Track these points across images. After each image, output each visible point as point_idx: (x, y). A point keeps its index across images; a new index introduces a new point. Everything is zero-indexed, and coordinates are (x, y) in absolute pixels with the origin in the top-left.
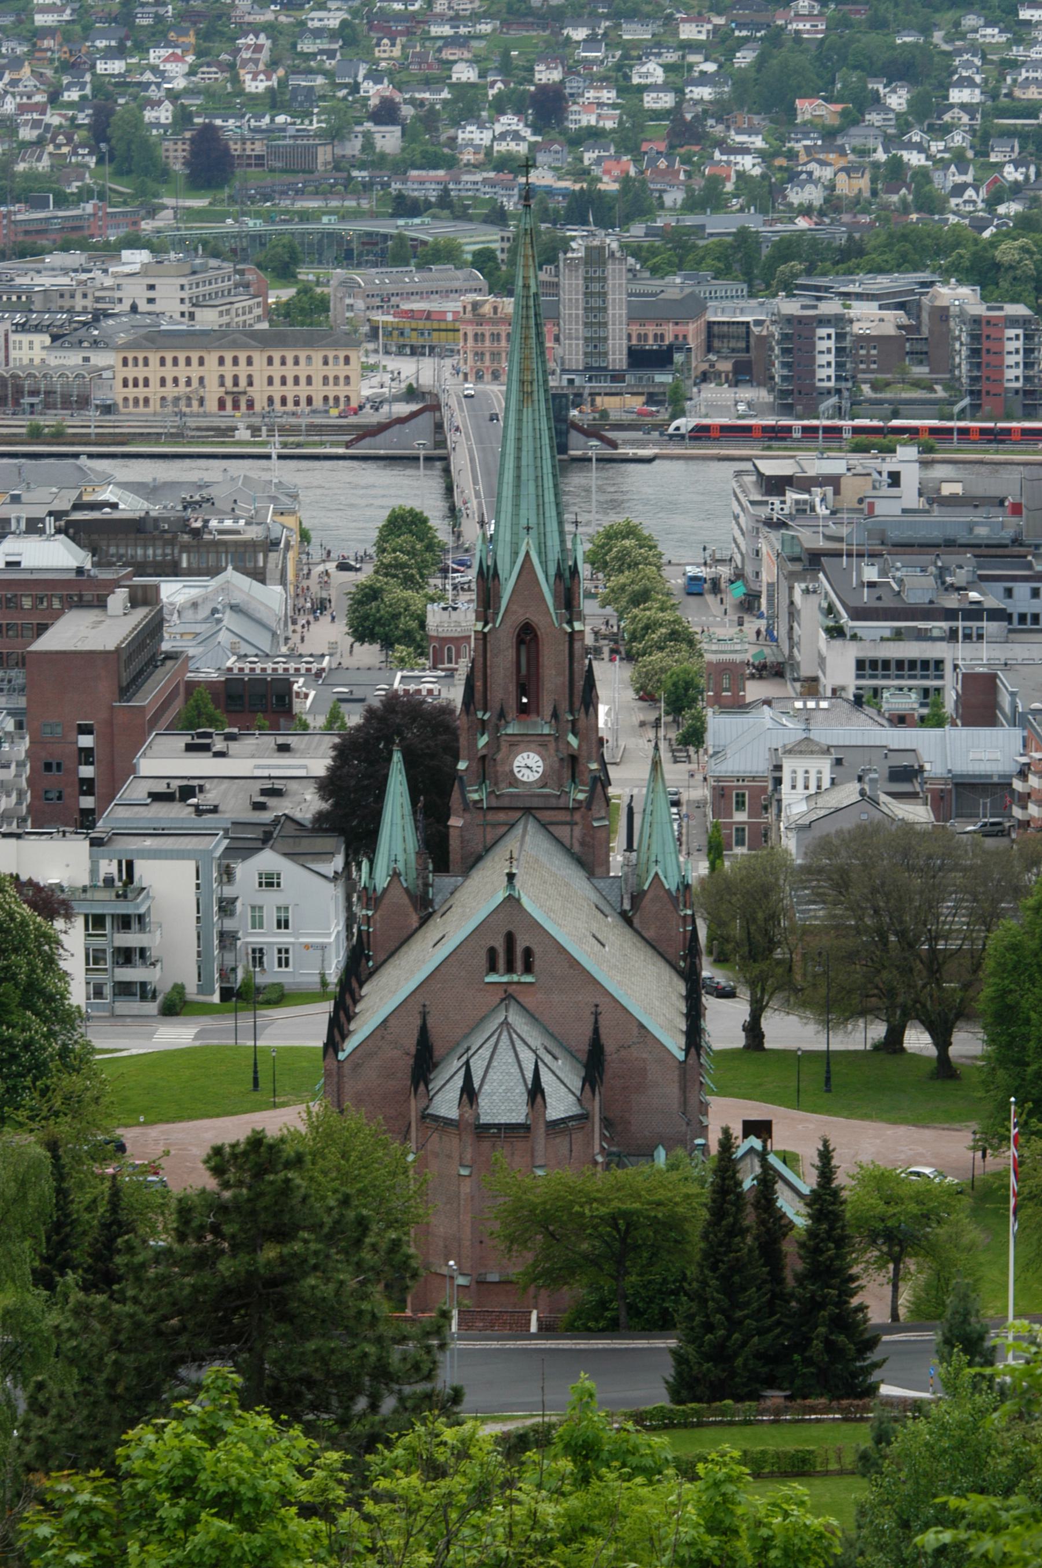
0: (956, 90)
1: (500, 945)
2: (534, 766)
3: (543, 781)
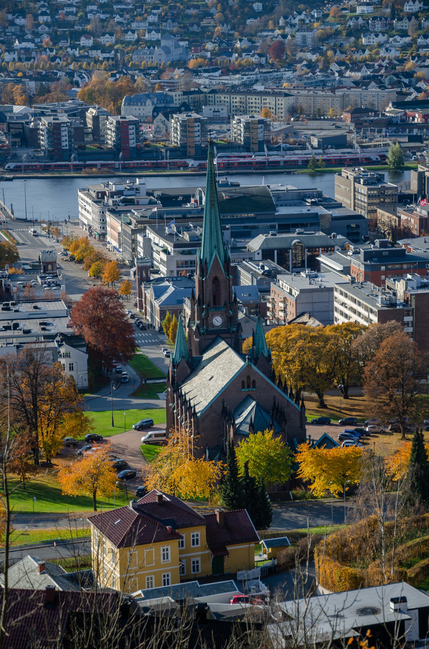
0: (41, 17)
1: (245, 379)
2: (219, 321)
3: (222, 325)
